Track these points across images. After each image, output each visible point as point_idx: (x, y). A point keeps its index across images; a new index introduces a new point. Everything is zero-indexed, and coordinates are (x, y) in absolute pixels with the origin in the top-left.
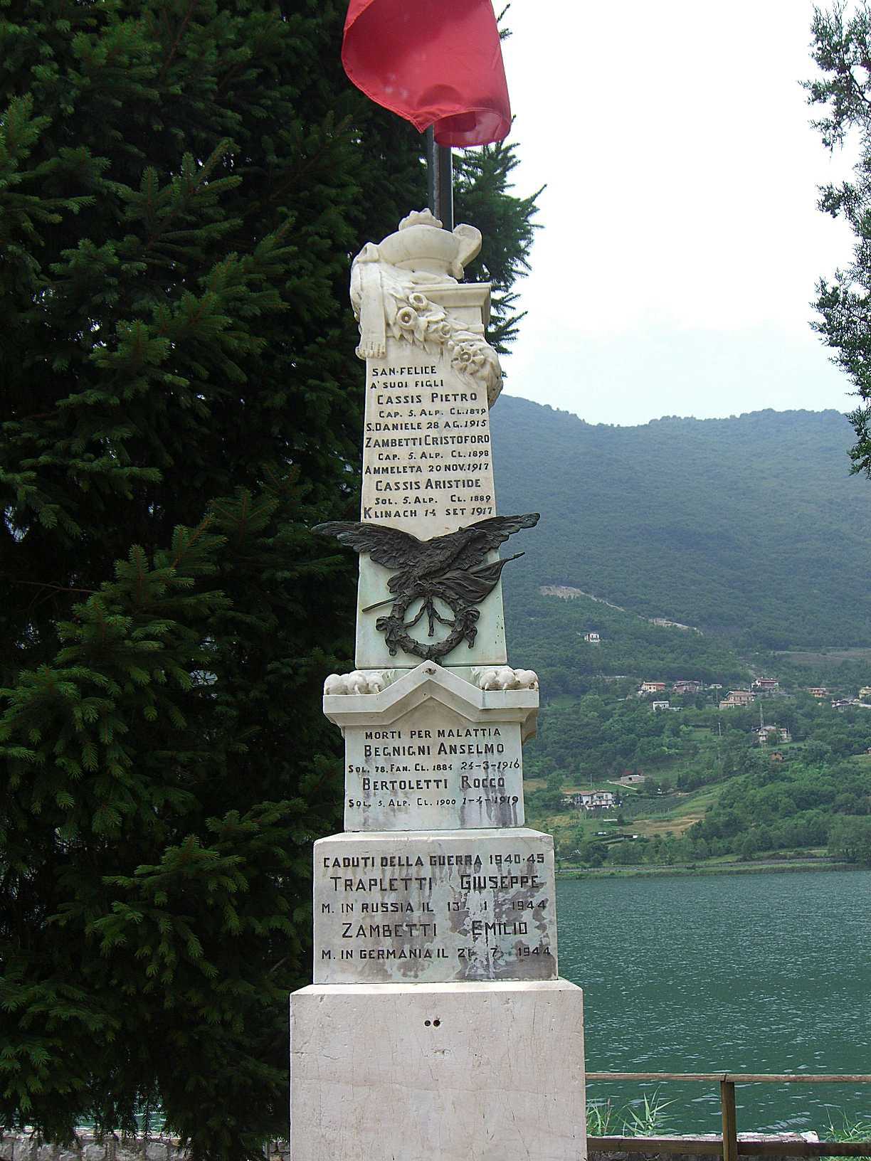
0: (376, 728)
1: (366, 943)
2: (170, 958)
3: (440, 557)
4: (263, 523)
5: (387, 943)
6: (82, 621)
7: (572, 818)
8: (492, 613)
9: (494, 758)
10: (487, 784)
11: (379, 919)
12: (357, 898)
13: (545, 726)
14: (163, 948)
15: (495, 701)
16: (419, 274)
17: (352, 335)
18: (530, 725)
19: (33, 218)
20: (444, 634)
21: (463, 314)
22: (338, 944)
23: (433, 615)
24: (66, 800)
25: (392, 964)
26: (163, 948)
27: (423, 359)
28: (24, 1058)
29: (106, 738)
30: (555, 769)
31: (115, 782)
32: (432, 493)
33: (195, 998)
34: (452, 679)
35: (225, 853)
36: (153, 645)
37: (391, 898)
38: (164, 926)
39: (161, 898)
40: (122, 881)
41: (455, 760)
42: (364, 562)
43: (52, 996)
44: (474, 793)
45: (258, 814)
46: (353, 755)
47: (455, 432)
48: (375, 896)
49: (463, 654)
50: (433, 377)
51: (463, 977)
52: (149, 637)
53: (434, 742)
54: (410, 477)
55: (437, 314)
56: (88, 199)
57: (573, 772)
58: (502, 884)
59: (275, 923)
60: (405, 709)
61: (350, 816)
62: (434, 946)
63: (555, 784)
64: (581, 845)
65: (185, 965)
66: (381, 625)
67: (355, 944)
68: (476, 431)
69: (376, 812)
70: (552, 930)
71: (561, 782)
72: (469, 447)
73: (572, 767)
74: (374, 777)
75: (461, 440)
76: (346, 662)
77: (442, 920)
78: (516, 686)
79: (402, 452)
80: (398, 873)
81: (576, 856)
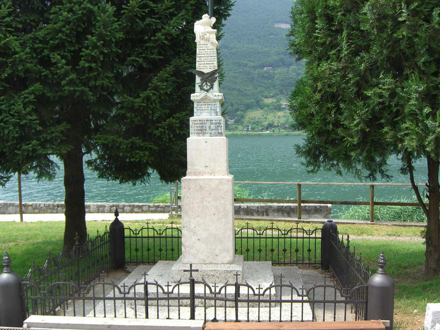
0: (199, 102)
1: (197, 132)
2: (168, 137)
3: (208, 76)
4: (181, 64)
5: (200, 132)
6: (152, 83)
7: (285, 113)
8: (216, 84)
9: (215, 106)
10: (214, 110)
11: (199, 128)
12: (196, 125)
13: (276, 78)
14: (166, 136)
15: (215, 98)
16: (205, 27)
17: (195, 38)
18: (220, 101)
19: (140, 14)
20: (208, 87)
21: (212, 35)
22: (193, 132)
23: (207, 84)
24: (150, 112)
25: (201, 134)
26: (166, 136)
27: (206, 43)
28: (144, 154)
29: (157, 102)
30: (279, 94)
31: (157, 109)
32: (207, 65)
33: (171, 144)
34: (210, 95)
35: (176, 120)
36: (164, 87)
37: (200, 126)
38: (167, 132)
39: (166, 127)
40: (160, 125)
41: (210, 106)
42: (197, 76)
43: (148, 144)
44: (212, 111)
45: (181, 114)
46: (195, 105)
47: (211, 55)
48: (198, 125)
49: (211, 90)
50: (208, 46)
51: (210, 136)
52: (164, 86)
53: (207, 104)
54: (204, 63)
55: (208, 35)
56: (149, 9)
57: (285, 96)
58: (216, 124)
59: (184, 132)
60: (202, 99)
61: (195, 114)
62: (206, 132)
63: (279, 100)
64: (288, 123)
65: (170, 139)
66: (199, 86)
67: (196, 132)
68: (214, 55)
69: (198, 114)
70: (223, 130)
71: (281, 99)
72: (213, 58)
73: (285, 94)
74: (198, 109)
75: (212, 56)
76: (194, 91)
77: (208, 128)
78: (218, 96)
79: (202, 58)
80: (201, 122)
81: (286, 127)
